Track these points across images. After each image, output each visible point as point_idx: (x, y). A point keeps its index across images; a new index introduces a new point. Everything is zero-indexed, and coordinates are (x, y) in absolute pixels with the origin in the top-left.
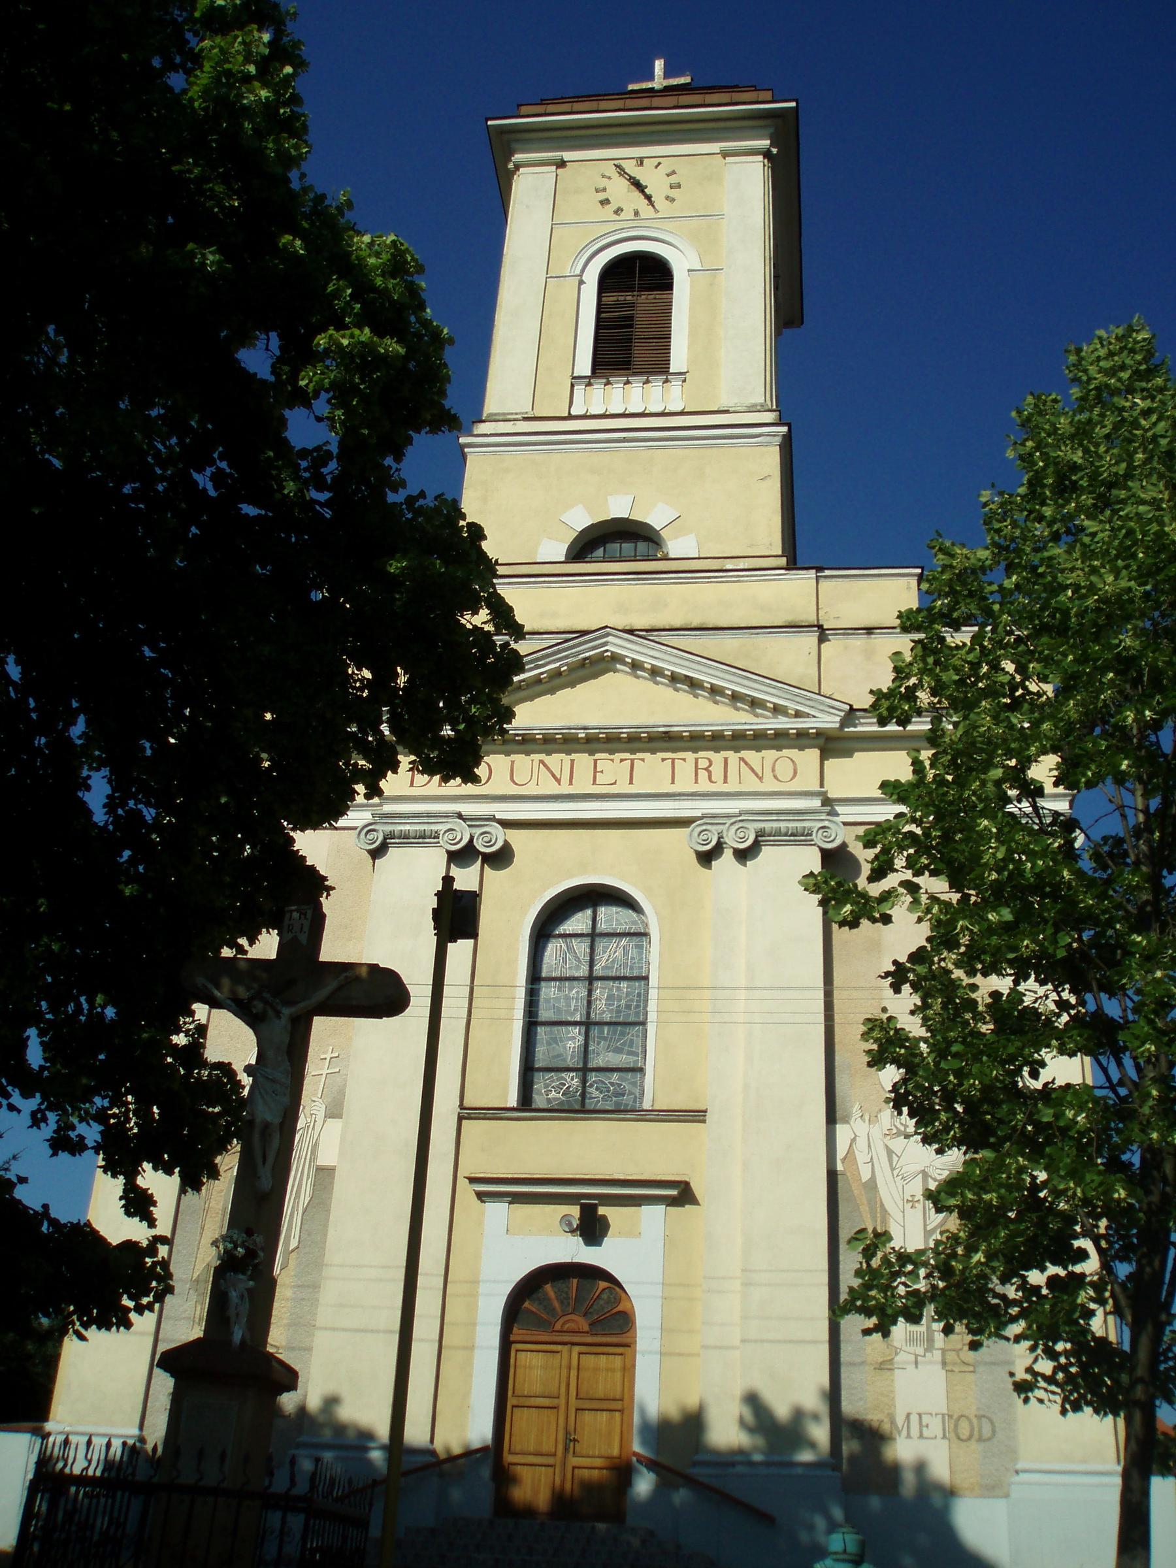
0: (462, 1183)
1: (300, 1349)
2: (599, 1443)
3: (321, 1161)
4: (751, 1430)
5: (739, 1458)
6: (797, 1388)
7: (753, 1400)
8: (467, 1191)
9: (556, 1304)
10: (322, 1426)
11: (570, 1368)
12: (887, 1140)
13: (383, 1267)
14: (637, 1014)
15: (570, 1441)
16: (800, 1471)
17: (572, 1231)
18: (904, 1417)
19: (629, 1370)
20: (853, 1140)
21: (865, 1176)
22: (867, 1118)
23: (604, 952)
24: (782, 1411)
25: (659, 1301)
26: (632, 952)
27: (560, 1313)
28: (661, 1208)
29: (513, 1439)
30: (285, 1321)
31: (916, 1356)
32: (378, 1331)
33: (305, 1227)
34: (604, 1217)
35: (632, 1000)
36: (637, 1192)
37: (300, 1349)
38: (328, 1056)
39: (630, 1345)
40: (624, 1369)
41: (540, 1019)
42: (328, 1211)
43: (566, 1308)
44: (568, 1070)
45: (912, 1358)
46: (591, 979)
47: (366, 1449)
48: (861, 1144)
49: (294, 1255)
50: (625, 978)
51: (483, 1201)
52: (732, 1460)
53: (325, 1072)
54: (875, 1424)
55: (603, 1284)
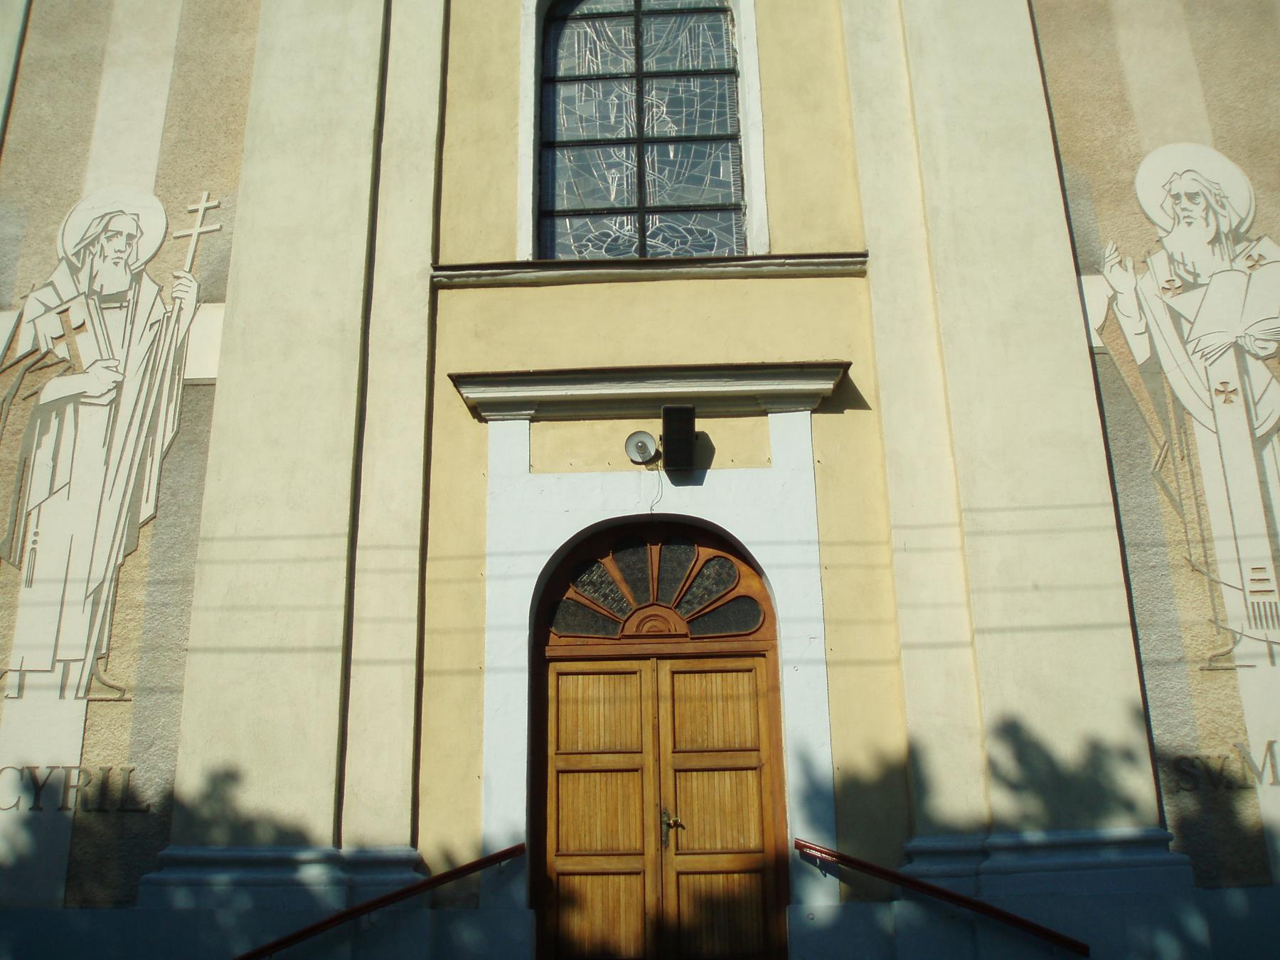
0: (444, 387)
1: (164, 690)
2: (722, 827)
3: (195, 370)
4: (1014, 787)
5: (997, 839)
6: (1084, 711)
7: (1011, 732)
8: (450, 401)
9: (625, 589)
10: (207, 824)
11: (657, 697)
12: (1167, 297)
13: (308, 537)
14: (722, 124)
15: (668, 825)
16: (1112, 856)
17: (649, 462)
18: (1264, 748)
19: (768, 698)
20: (1113, 299)
21: (1141, 353)
22: (1130, 265)
23: (658, 38)
24: (1066, 747)
25: (815, 573)
26: (705, 36)
27: (634, 606)
28: (801, 419)
29: (563, 829)
30: (135, 644)
31: (1270, 643)
32: (303, 650)
33: (167, 482)
34: (704, 436)
35: (712, 105)
36: (766, 387)
37: (164, 690)
38: (202, 206)
39: (764, 653)
40: (756, 694)
41: (559, 139)
42: (206, 453)
43: (655, 594)
44: (613, 212)
45: (1263, 648)
46: (640, 77)
47: (295, 865)
48: (1126, 304)
49: (147, 530)
50: (696, 73)
51: (483, 420)
52: (984, 839)
53: (196, 231)
54: (1215, 764)
55: (705, 553)
